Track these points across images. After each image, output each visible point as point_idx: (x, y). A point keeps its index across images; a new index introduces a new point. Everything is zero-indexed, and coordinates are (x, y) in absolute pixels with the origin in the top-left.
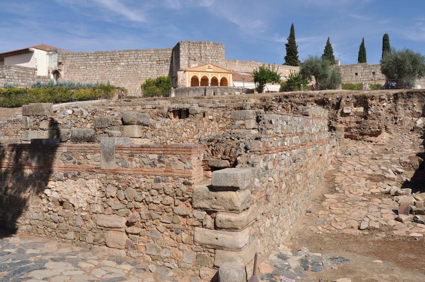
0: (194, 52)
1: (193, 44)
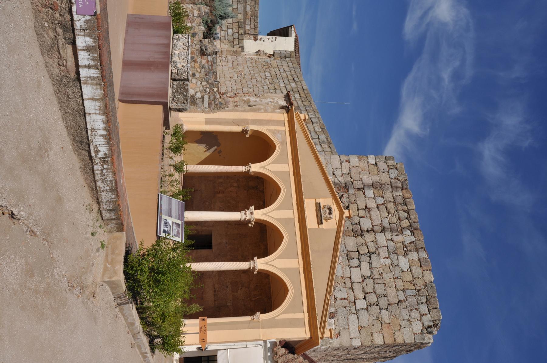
0: (372, 204)
1: (400, 200)
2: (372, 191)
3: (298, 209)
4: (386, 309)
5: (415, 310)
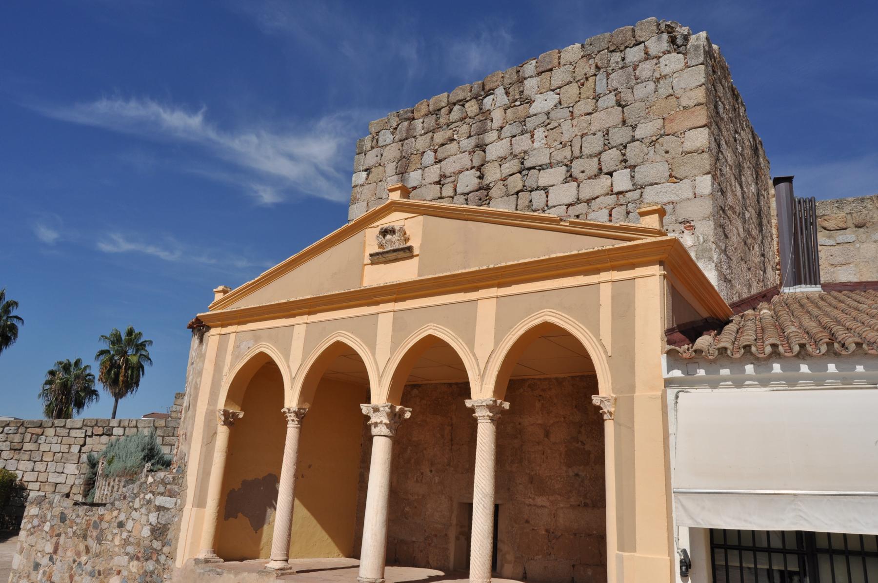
0: (433, 173)
1: (431, 121)
2: (412, 174)
3: (377, 303)
4: (634, 128)
5: (637, 72)
